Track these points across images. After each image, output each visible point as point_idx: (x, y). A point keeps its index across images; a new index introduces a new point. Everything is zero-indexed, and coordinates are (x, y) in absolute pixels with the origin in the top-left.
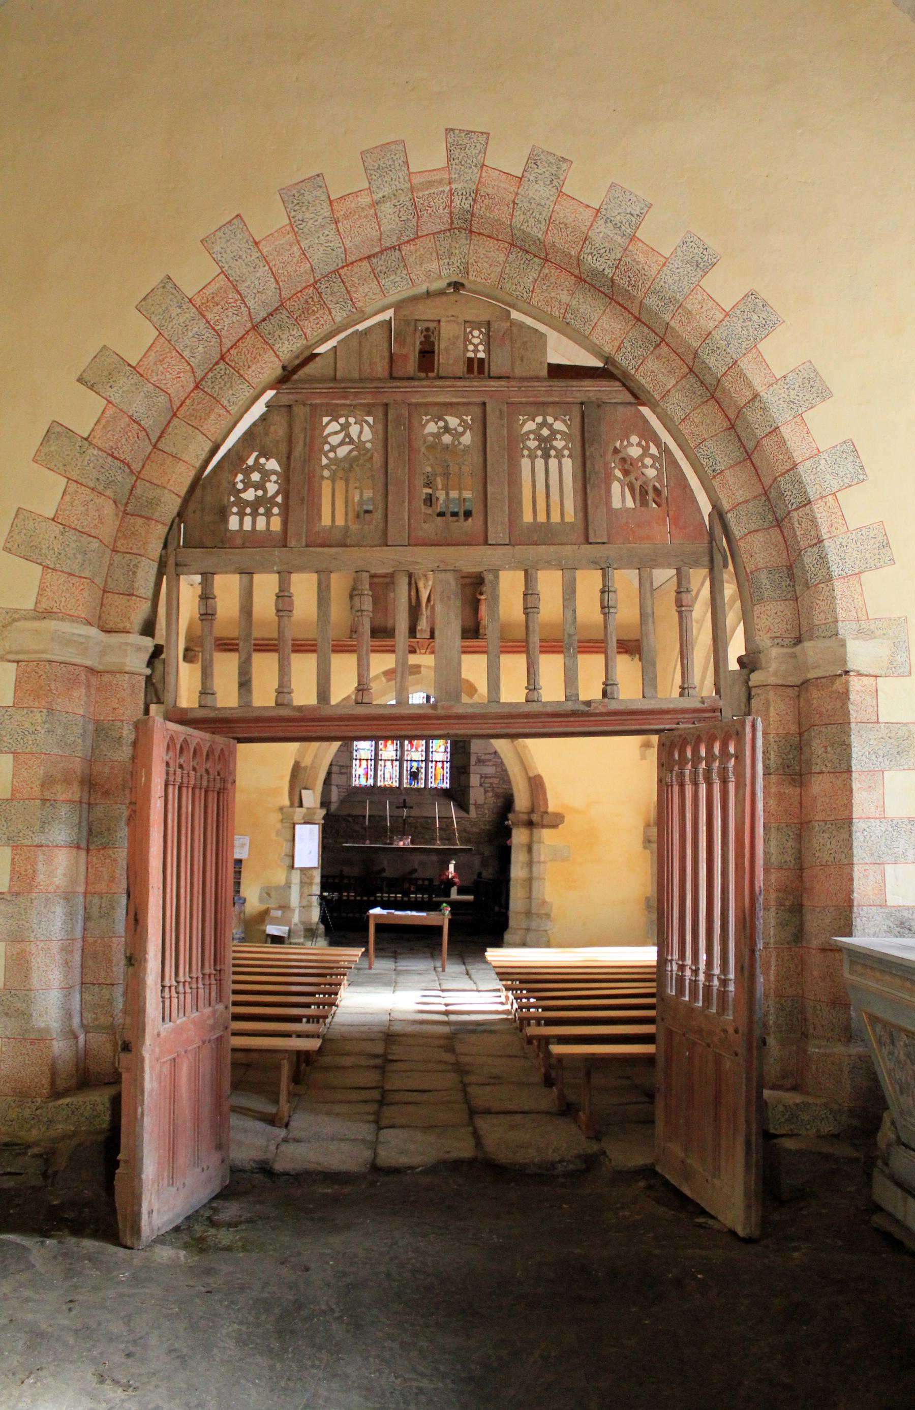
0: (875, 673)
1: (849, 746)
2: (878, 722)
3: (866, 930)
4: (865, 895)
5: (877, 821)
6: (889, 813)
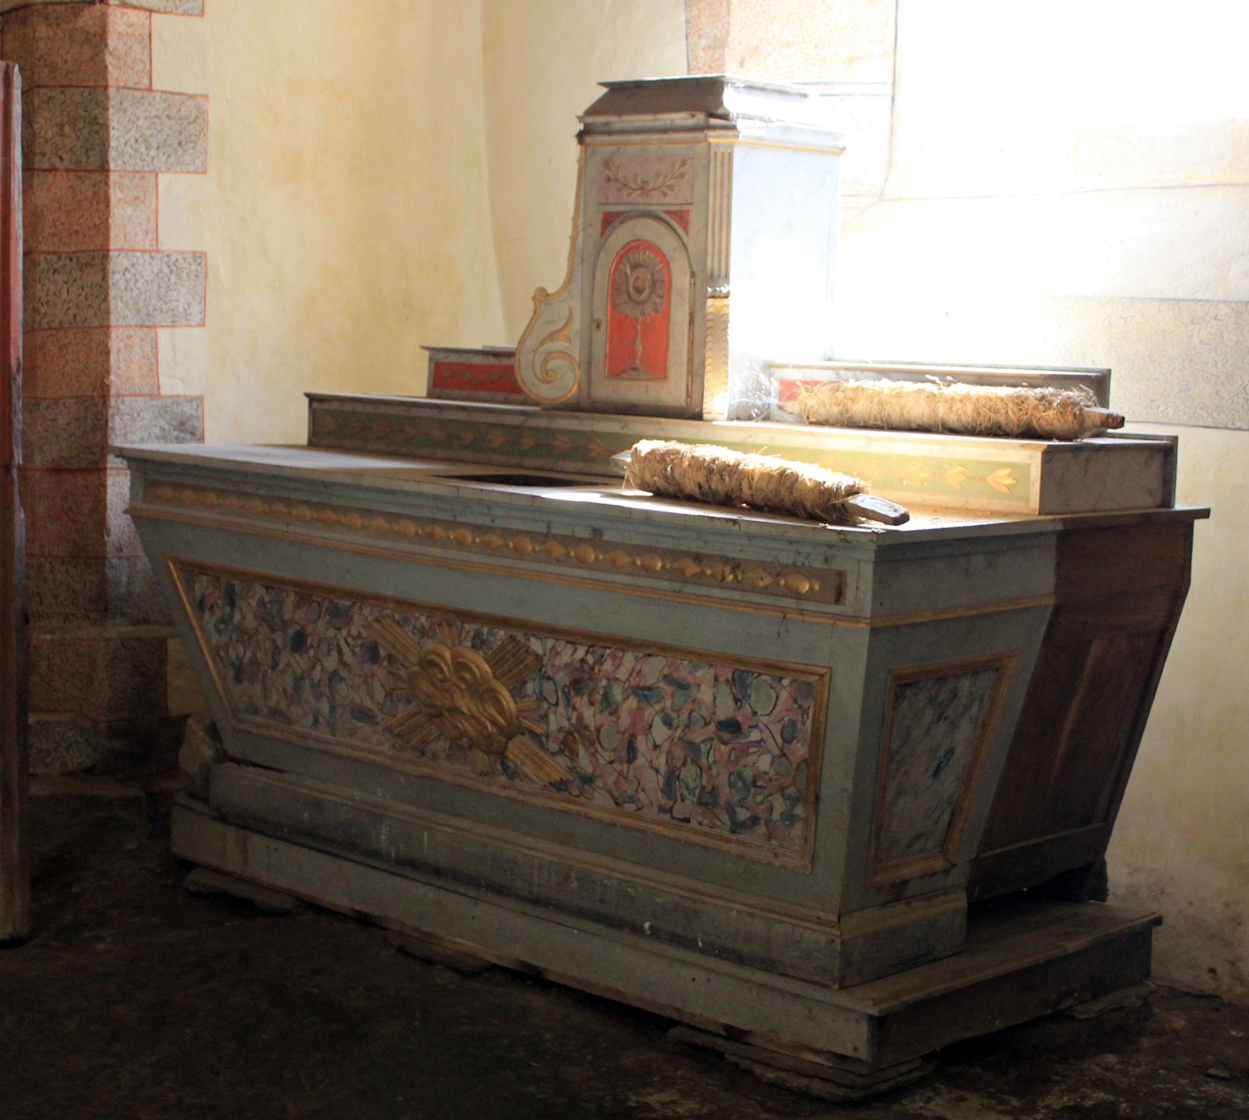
0: (149, 6)
1: (105, 127)
2: (150, 89)
3: (129, 436)
4: (128, 379)
5: (147, 256)
6: (167, 244)
